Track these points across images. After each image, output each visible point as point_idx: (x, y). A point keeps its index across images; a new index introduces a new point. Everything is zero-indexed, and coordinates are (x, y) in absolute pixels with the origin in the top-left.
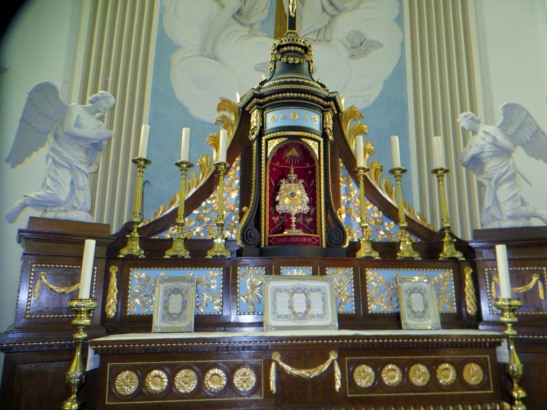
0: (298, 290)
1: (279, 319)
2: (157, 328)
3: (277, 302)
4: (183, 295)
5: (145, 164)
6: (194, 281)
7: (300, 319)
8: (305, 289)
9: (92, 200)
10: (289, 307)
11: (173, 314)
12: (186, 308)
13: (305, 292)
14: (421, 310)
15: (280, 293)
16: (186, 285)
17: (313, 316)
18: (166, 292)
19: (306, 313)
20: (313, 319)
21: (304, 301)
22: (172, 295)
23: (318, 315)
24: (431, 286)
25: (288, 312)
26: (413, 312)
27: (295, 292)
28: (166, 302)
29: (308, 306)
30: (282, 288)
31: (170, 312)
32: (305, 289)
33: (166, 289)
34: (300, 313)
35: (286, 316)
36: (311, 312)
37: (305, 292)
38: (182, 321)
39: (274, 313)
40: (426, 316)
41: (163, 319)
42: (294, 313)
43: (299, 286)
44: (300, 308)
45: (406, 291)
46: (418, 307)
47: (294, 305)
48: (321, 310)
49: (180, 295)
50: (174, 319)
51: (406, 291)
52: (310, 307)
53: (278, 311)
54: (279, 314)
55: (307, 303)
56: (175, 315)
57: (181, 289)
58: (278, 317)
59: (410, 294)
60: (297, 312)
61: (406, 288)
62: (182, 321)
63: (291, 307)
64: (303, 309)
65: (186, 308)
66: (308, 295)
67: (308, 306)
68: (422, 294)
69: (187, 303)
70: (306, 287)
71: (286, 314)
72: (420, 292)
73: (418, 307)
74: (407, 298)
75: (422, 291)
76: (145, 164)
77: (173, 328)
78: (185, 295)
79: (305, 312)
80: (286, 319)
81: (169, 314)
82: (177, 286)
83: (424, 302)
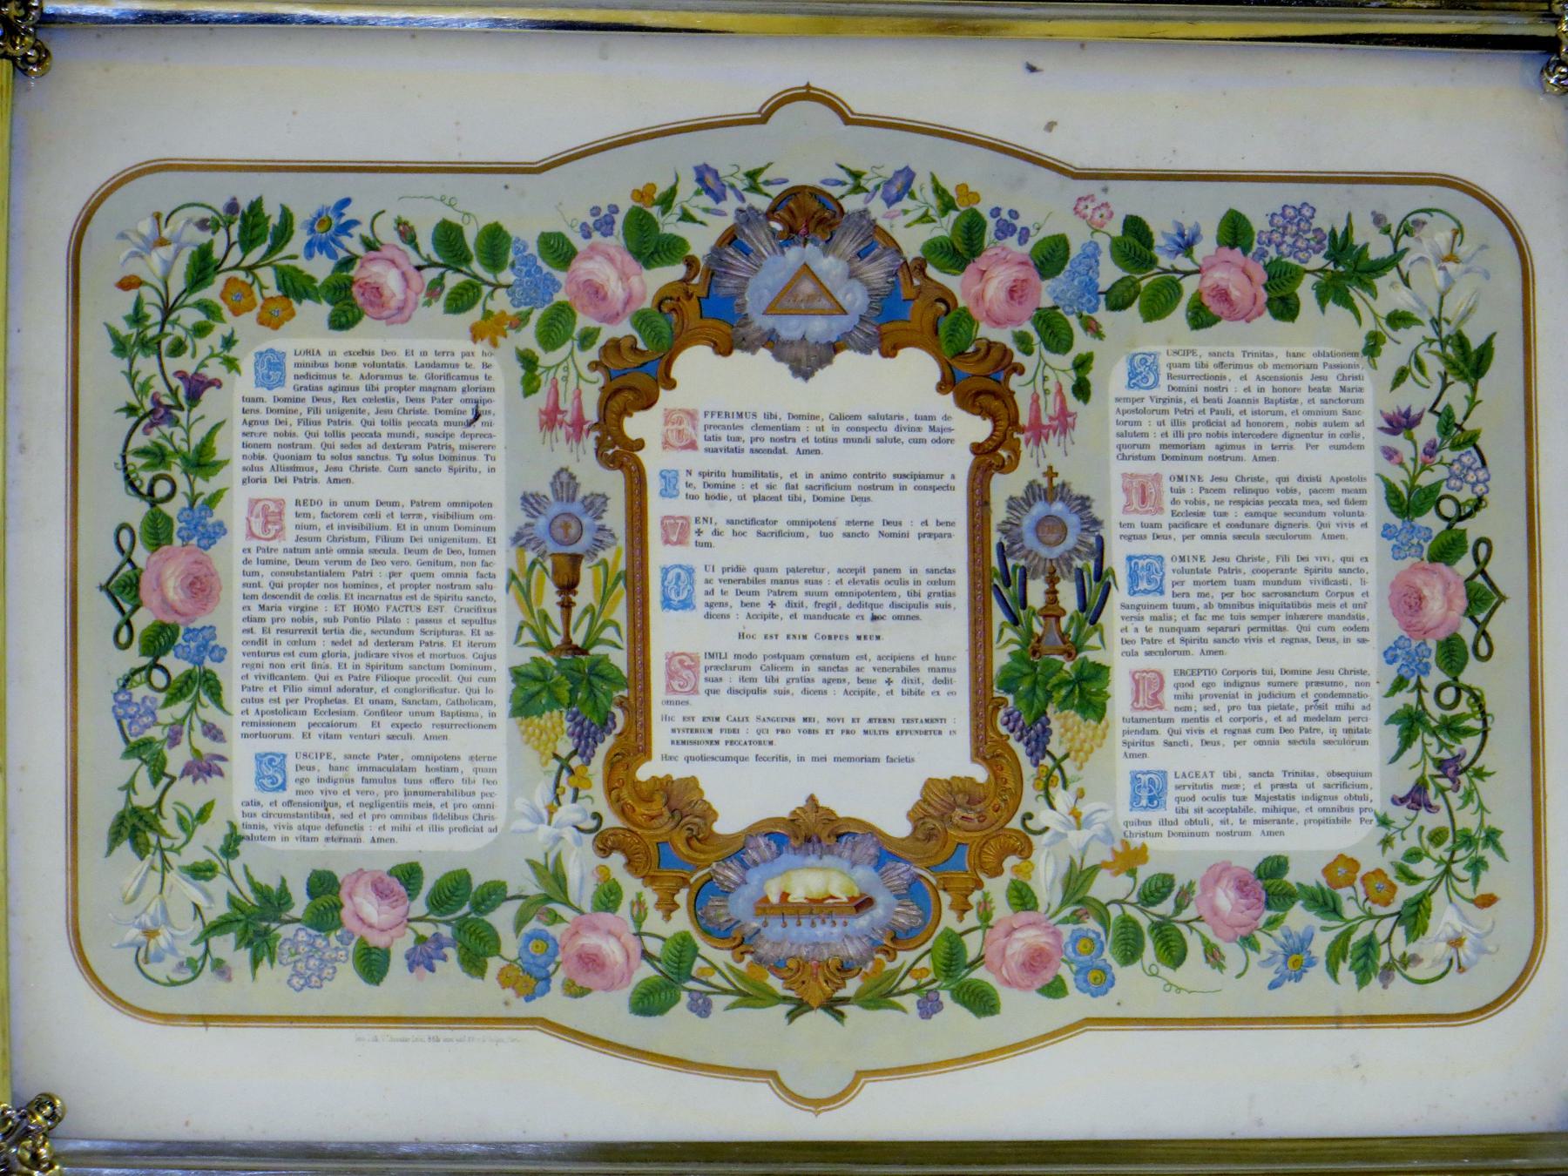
1: (269, 986)
3: (232, 556)
7: (818, 989)
8: (963, 248)
10: (532, 691)
13: (972, 309)
15: (307, 332)
17: (1154, 926)
19: (964, 833)
20: (1138, 985)
21: (932, 541)
22: (696, 365)
23: (1270, 883)
25: (503, 803)
27: (708, 310)
29: (1039, 679)
30: (372, 203)
31: (682, 806)
32: (963, 248)
34: (813, 831)
35: (460, 912)
36: (1088, 810)
37: (972, 309)
38: (1021, 1009)
39: (134, 828)
42: (664, 835)
43: (805, 156)
44: (816, 695)
47: (670, 633)
48: (1375, 763)
52: (1087, 692)
53: (238, 788)
54: (283, 856)
55: (995, 581)
58: (255, 922)
60: (739, 800)
62: (1021, 1009)
63: (584, 693)
64: (895, 748)
66: (1037, 381)
67: (1039, 679)
71: (439, 848)
80: (449, 984)
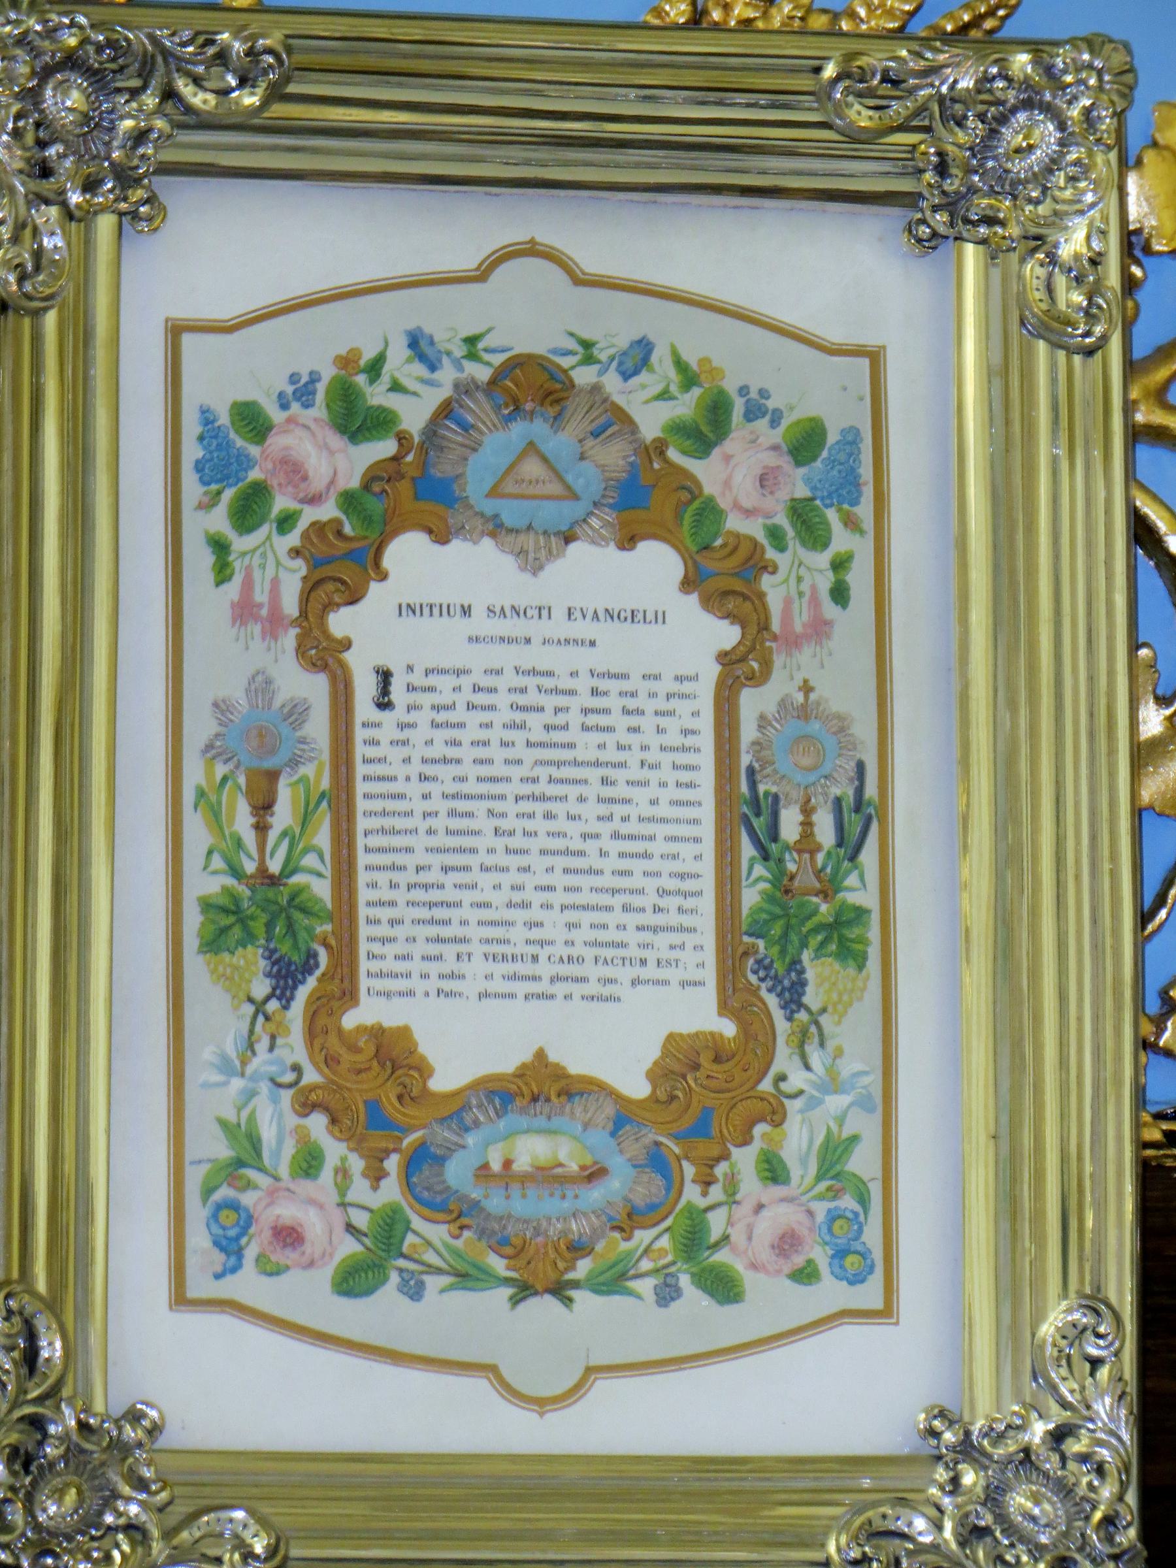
0: (498, 444)
7: (543, 1273)
8: (708, 429)
14: (628, 1028)
24: (1028, 326)
26: (374, 1092)
27: (414, 491)
31: (394, 1054)
40: (752, 1218)
45: (230, 462)
46: (549, 952)
51: (230, 462)
59: (342, 566)
60: (461, 1046)
61: (221, 377)
62: (770, 1299)
65: (843, 936)
68: (726, 577)
70: (739, 359)
72: (648, 500)
73: (549, 952)
74: (234, 661)
75: (737, 479)
79: (682, 1060)
83: (748, 812)
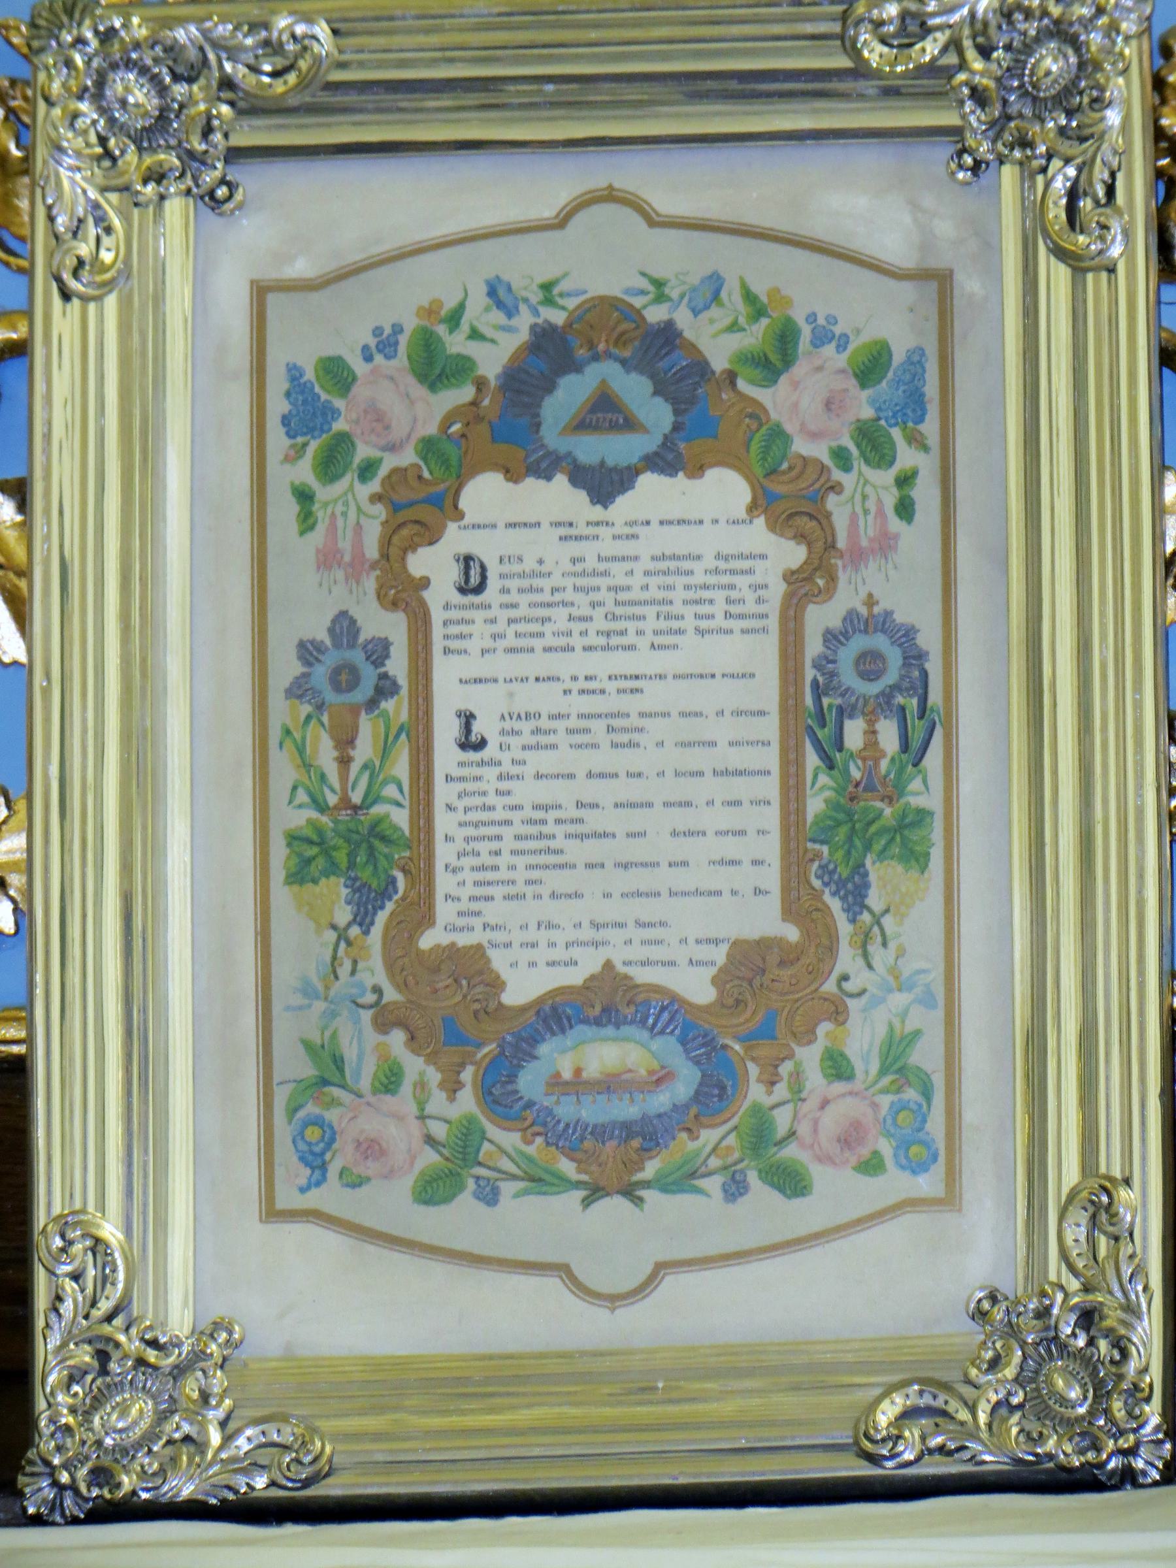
2: (166, 1369)
4: (792, 500)
5: (541, 303)
6: (1078, 98)
9: (103, 333)
11: (556, 1014)
12: (907, 839)
16: (871, 204)
18: (310, 414)
22: (485, 494)
28: (350, 685)
31: (470, 968)
33: (299, 344)
38: (836, 1190)
41: (307, 1138)
43: (612, 1236)
49: (725, 490)
50: (616, 1158)
56: (603, 1053)
57: (718, 343)
62: (836, 1190)
65: (907, 839)
69: (923, 721)
76: (541, 303)
77: (637, 1379)
78: (859, 500)
81: (460, 1018)
82: (603, 264)
